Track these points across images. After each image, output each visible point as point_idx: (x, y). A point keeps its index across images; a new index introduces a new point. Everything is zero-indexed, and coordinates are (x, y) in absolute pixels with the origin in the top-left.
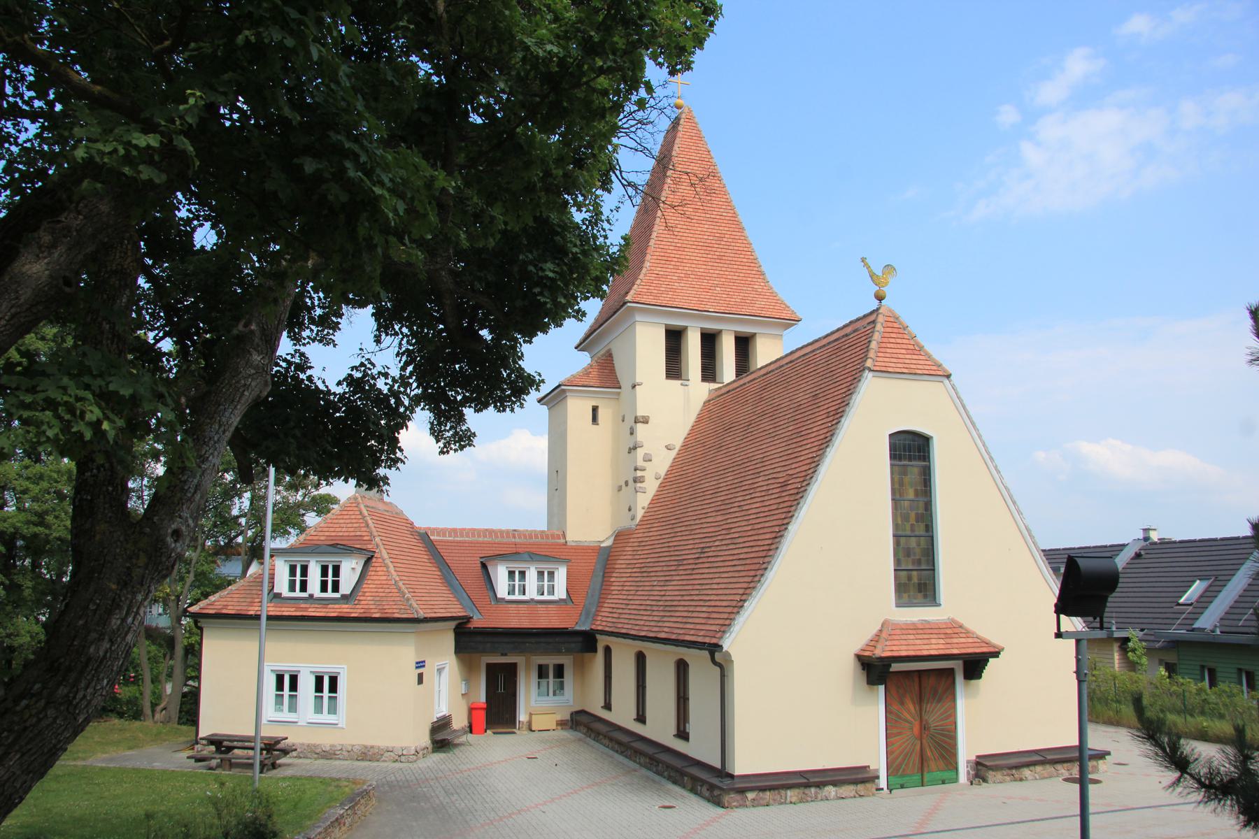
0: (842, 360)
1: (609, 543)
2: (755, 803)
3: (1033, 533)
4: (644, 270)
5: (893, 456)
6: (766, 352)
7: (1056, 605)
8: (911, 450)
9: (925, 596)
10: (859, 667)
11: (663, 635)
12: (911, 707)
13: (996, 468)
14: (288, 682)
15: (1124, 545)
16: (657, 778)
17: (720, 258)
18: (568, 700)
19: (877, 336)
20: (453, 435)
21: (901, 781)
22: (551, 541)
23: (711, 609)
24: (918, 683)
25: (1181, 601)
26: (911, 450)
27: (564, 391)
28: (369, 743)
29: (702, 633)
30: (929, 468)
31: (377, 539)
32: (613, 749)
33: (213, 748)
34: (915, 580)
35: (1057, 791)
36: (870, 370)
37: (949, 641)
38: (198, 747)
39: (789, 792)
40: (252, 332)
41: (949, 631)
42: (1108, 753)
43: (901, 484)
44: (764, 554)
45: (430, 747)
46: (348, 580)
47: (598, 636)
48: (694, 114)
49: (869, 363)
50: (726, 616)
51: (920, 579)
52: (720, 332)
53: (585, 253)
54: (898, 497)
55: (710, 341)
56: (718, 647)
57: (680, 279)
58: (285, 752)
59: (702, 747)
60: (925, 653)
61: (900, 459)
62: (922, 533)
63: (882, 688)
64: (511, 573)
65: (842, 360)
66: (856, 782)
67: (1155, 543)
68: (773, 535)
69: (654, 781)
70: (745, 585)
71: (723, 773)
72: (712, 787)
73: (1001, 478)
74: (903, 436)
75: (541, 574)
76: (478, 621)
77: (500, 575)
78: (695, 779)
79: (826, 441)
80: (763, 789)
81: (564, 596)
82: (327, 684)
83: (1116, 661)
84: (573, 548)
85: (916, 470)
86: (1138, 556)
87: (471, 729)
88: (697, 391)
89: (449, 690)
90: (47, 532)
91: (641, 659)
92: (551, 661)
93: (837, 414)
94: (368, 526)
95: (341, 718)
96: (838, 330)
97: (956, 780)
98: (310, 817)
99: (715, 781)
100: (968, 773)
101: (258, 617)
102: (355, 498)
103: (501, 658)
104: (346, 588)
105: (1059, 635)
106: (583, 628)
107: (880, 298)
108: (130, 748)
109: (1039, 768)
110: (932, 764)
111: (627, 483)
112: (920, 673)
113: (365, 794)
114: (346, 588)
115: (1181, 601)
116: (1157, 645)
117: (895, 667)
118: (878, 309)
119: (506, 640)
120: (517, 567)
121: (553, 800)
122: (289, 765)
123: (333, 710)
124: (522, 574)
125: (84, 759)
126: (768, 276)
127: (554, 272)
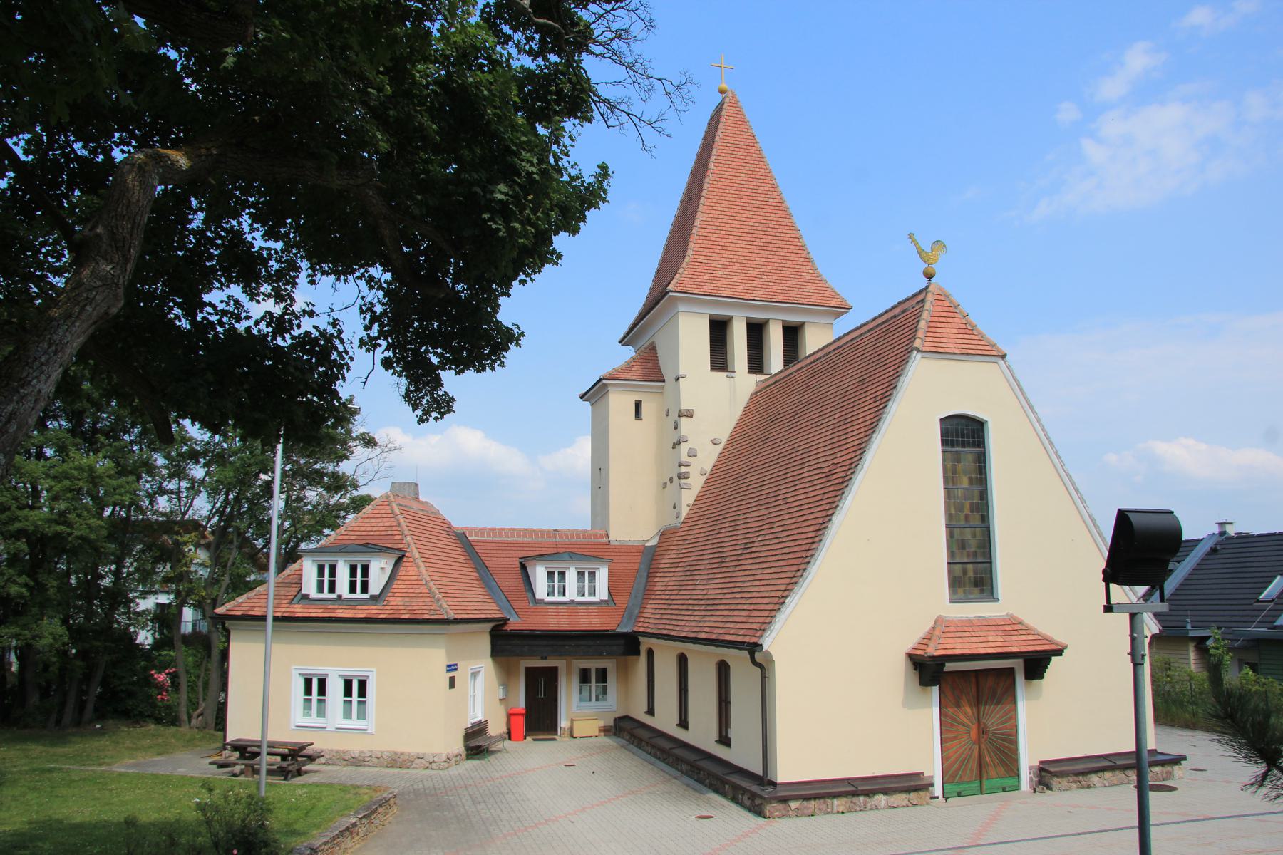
0: (888, 344)
1: (654, 542)
2: (799, 813)
3: (1098, 523)
4: (687, 259)
5: (945, 443)
6: (814, 340)
7: (1104, 572)
8: (964, 435)
9: (982, 591)
10: (910, 664)
11: (703, 636)
12: (968, 709)
13: (1056, 453)
14: (315, 686)
15: (1199, 541)
16: (698, 786)
17: (766, 245)
18: (613, 705)
19: (925, 315)
20: (427, 398)
21: (957, 788)
22: (593, 540)
23: (752, 607)
24: (974, 684)
25: (1261, 597)
26: (964, 435)
27: (605, 385)
28: (399, 749)
29: (742, 632)
30: (984, 454)
31: (409, 538)
32: (655, 756)
33: (237, 754)
34: (971, 574)
35: (1117, 798)
36: (919, 351)
37: (1008, 638)
38: (226, 753)
39: (836, 801)
40: (98, 235)
41: (1007, 628)
42: (1184, 758)
43: (954, 472)
44: (807, 547)
45: (464, 752)
46: (377, 580)
47: (641, 639)
48: (738, 98)
49: (917, 343)
50: (766, 613)
51: (975, 572)
52: (767, 321)
53: (544, 173)
54: (951, 485)
55: (756, 331)
56: (757, 646)
57: (725, 267)
58: (311, 759)
59: (743, 754)
60: (982, 651)
61: (953, 446)
62: (978, 523)
63: (936, 689)
64: (550, 574)
65: (888, 344)
66: (908, 790)
67: (1232, 538)
68: (817, 527)
69: (695, 790)
70: (787, 581)
71: (765, 781)
72: (753, 796)
73: (1062, 464)
74: (955, 421)
75: (581, 574)
76: (515, 623)
77: (539, 574)
78: (736, 788)
79: (872, 427)
80: (807, 798)
81: (605, 597)
82: (356, 688)
83: (1192, 662)
84: (616, 548)
85: (970, 458)
86: (1213, 551)
87: (510, 735)
88: (743, 383)
89: (484, 694)
90: (69, 530)
91: (683, 660)
92: (593, 664)
93: (884, 399)
94: (399, 524)
95: (369, 724)
96: (886, 312)
97: (1018, 787)
98: (318, 826)
99: (755, 788)
100: (1031, 780)
101: (263, 618)
102: (388, 497)
103: (541, 664)
104: (375, 589)
105: (1108, 608)
106: (625, 630)
107: (929, 276)
108: (159, 754)
109: (1108, 775)
110: (992, 771)
111: (671, 480)
112: (977, 673)
113: (385, 803)
114: (375, 589)
115: (1261, 597)
116: (1236, 645)
117: (950, 667)
118: (924, 290)
119: (545, 643)
120: (556, 566)
121: (584, 809)
122: (316, 772)
123: (362, 715)
124: (562, 574)
125: (109, 764)
126: (817, 263)
127: (506, 194)
